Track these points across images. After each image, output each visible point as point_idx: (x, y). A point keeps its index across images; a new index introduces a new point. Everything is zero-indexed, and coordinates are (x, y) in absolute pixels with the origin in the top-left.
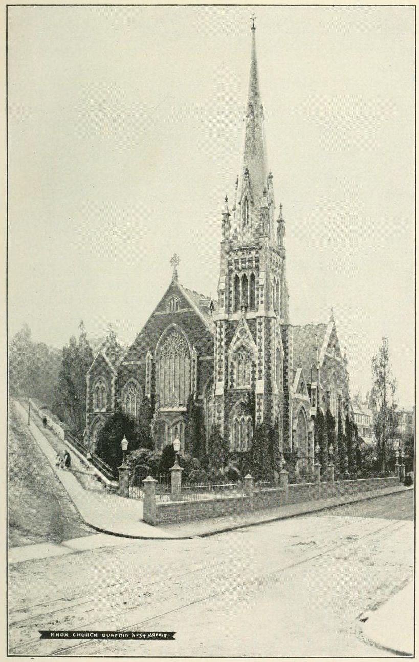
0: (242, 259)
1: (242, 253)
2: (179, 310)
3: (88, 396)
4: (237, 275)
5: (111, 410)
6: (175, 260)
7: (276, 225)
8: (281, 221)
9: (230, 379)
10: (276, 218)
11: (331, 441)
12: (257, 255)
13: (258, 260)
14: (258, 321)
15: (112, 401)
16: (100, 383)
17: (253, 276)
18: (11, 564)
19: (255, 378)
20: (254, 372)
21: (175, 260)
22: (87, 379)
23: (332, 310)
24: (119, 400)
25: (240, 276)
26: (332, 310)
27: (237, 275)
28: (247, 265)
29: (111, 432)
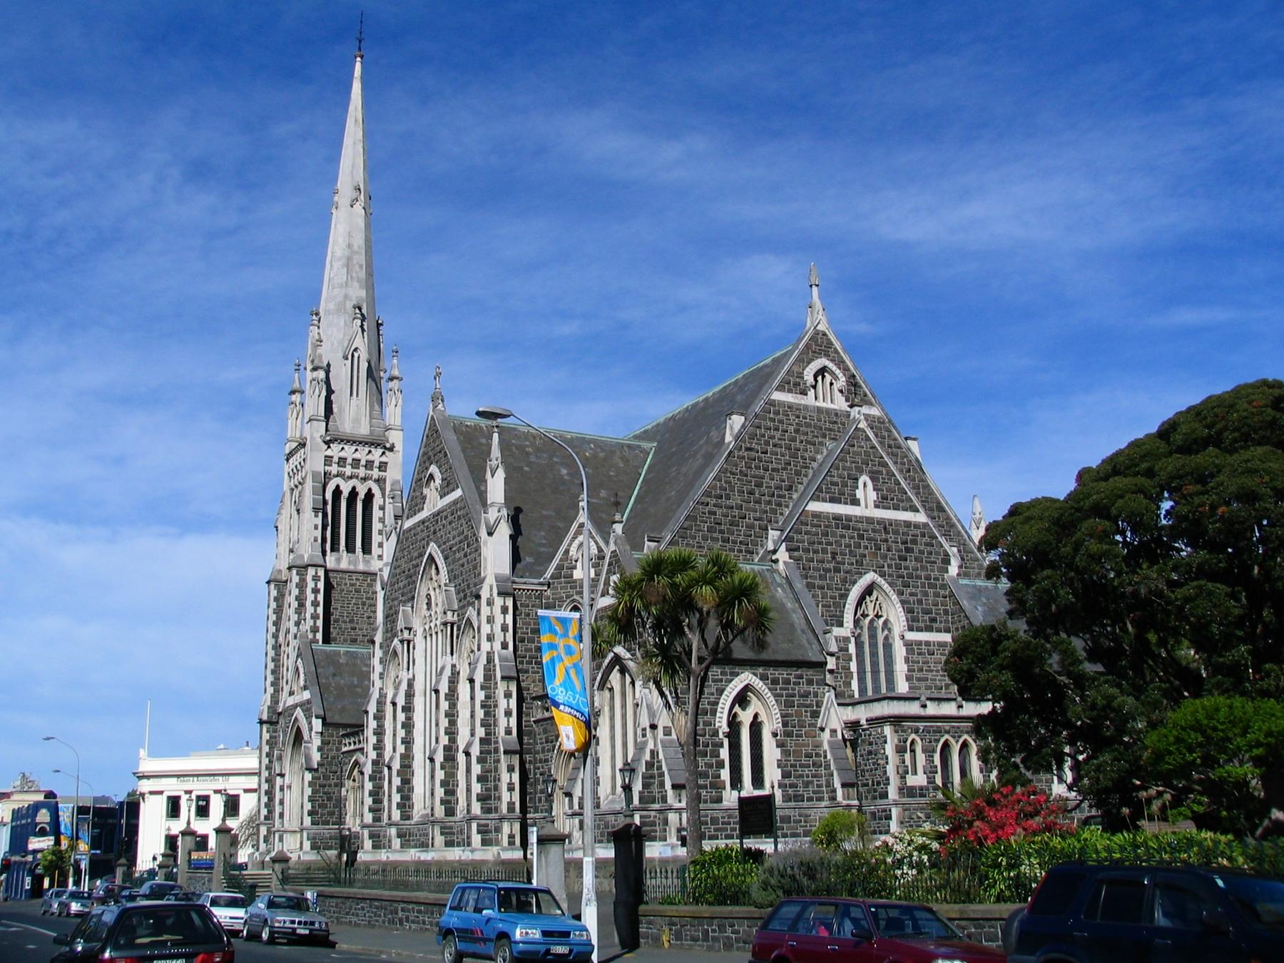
0: (353, 460)
1: (367, 449)
4: (338, 487)
9: (319, 618)
12: (384, 459)
13: (383, 466)
17: (369, 496)
18: (676, 755)
19: (311, 631)
25: (346, 489)
27: (338, 487)
28: (348, 470)
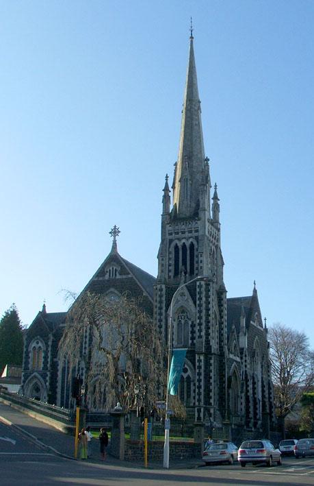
2: (118, 277)
3: (24, 355)
5: (47, 369)
6: (115, 232)
7: (212, 201)
8: (216, 198)
10: (212, 196)
11: (138, 395)
14: (198, 283)
15: (49, 360)
16: (37, 343)
20: (193, 332)
21: (115, 232)
22: (24, 339)
23: (255, 284)
24: (55, 360)
26: (255, 284)
29: (235, 425)
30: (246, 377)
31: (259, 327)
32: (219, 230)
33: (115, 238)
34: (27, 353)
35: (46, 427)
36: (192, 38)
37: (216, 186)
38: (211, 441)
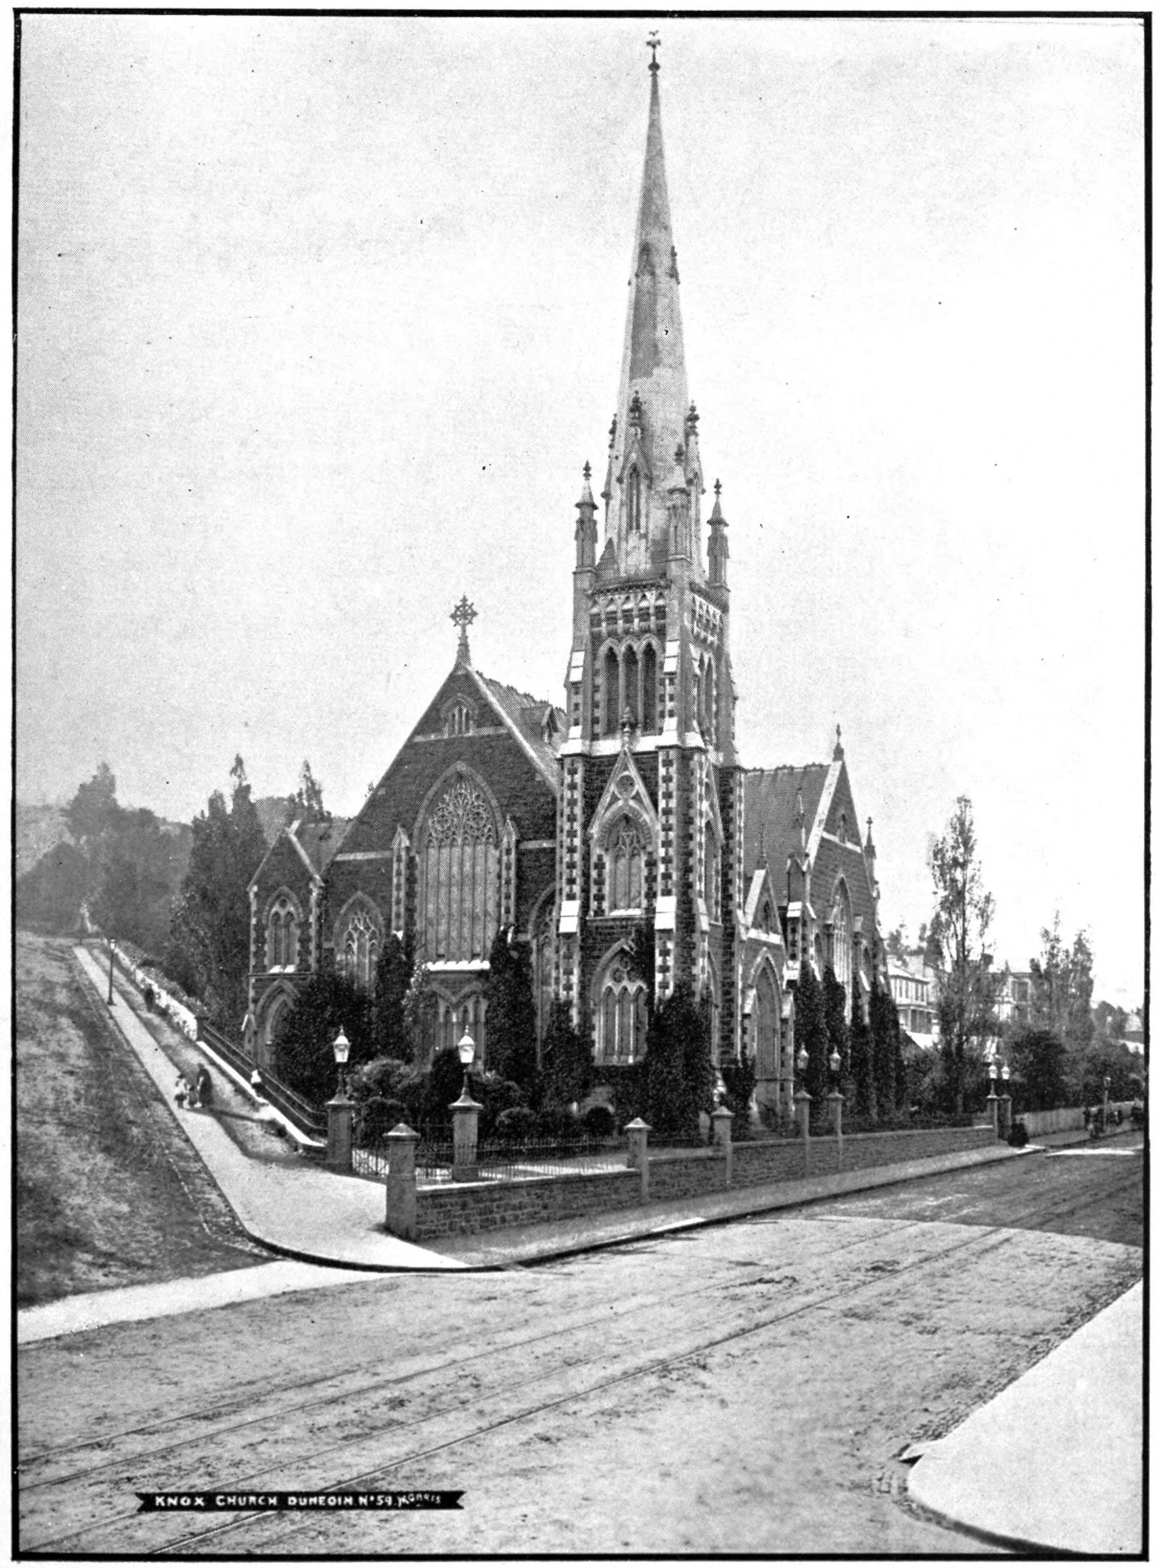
7: (706, 531)
8: (717, 522)
10: (706, 514)
21: (464, 613)
30: (856, 1486)
31: (849, 845)
32: (725, 608)
33: (464, 631)
34: (260, 928)
35: (566, 1161)
36: (654, 66)
37: (718, 486)
38: (931, 1100)
